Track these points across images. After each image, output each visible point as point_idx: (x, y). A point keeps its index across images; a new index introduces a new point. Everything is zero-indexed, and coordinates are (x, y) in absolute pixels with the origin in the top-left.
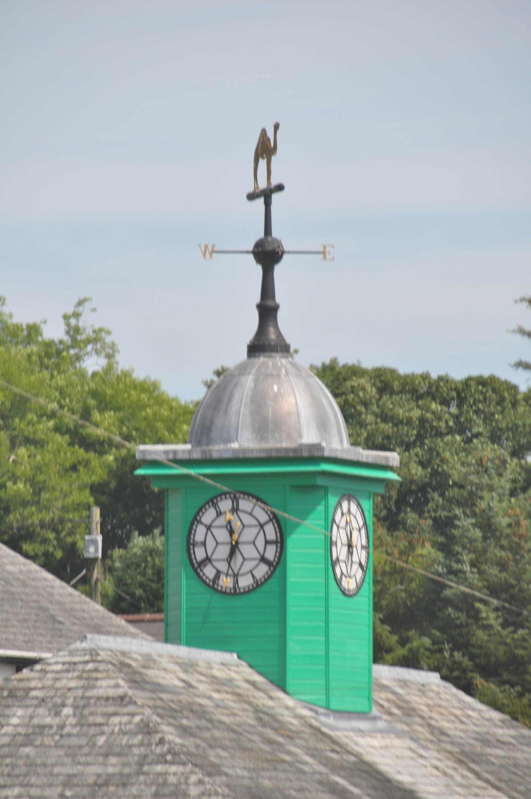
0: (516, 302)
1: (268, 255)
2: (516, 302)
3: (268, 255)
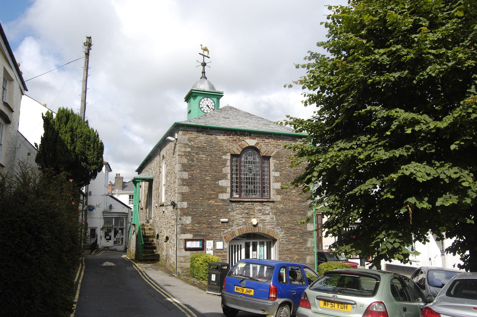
0: (200, 54)
1: (204, 65)
2: (200, 54)
3: (204, 65)
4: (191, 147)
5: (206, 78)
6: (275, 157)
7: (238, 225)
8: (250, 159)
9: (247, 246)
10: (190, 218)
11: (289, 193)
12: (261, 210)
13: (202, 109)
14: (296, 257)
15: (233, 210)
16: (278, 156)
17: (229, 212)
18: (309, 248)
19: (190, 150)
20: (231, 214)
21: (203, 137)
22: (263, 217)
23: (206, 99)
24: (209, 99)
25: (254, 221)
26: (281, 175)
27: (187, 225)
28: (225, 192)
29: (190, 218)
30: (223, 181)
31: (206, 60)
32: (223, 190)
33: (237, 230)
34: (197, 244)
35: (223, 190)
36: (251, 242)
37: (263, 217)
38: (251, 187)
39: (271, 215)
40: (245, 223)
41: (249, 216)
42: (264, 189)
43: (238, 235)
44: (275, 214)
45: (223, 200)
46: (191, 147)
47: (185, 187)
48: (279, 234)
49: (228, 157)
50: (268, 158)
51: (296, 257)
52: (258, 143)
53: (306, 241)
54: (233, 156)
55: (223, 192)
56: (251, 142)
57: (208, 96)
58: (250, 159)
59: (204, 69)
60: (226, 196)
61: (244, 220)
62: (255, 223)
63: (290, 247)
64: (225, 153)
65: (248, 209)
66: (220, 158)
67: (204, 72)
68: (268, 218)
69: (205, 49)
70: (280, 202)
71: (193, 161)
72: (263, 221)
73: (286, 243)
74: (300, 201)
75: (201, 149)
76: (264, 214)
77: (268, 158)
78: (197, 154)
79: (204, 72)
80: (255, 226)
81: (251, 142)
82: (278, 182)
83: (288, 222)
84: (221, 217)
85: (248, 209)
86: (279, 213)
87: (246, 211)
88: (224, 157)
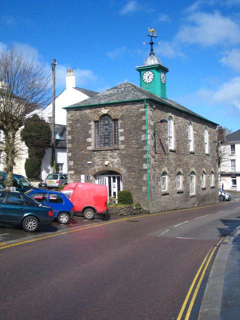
4: (72, 120)
5: (154, 54)
7: (98, 165)
9: (110, 178)
14: (135, 187)
16: (122, 118)
17: (92, 158)
19: (71, 122)
21: (78, 113)
22: (112, 160)
23: (147, 72)
24: (149, 72)
25: (106, 163)
26: (124, 131)
27: (71, 166)
30: (89, 138)
32: (89, 144)
33: (97, 168)
35: (89, 144)
36: (111, 176)
37: (112, 160)
38: (107, 141)
39: (118, 159)
40: (102, 164)
41: (104, 159)
42: (116, 141)
43: (97, 171)
44: (120, 157)
46: (72, 120)
48: (123, 171)
50: (116, 120)
51: (135, 187)
55: (90, 145)
56: (104, 111)
58: (106, 122)
59: (152, 47)
61: (101, 162)
62: (106, 164)
63: (131, 180)
64: (90, 121)
68: (116, 161)
72: (112, 162)
73: (128, 177)
74: (138, 148)
75: (77, 121)
77: (116, 120)
78: (75, 124)
80: (107, 166)
81: (104, 111)
83: (130, 163)
84: (88, 161)
86: (123, 157)
88: (90, 124)
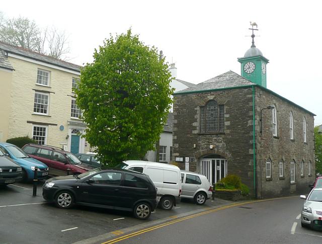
1: (253, 36)
6: (227, 105)
8: (212, 108)
10: (178, 144)
11: (236, 128)
12: (216, 140)
13: (254, 68)
15: (200, 140)
16: (228, 104)
18: (250, 166)
20: (199, 142)
28: (196, 130)
29: (178, 144)
31: (255, 33)
32: (195, 128)
34: (181, 159)
35: (195, 128)
40: (206, 148)
41: (209, 144)
45: (195, 134)
47: (176, 128)
49: (198, 108)
52: (215, 97)
53: (248, 161)
54: (201, 107)
57: (250, 61)
58: (212, 108)
60: (196, 132)
63: (236, 164)
64: (196, 107)
65: (208, 139)
66: (194, 109)
67: (253, 42)
68: (221, 145)
69: (255, 24)
70: (228, 134)
71: (179, 113)
72: (217, 146)
76: (218, 142)
79: (253, 42)
82: (228, 121)
85: (208, 139)
86: (228, 142)
87: (207, 140)
88: (196, 109)
